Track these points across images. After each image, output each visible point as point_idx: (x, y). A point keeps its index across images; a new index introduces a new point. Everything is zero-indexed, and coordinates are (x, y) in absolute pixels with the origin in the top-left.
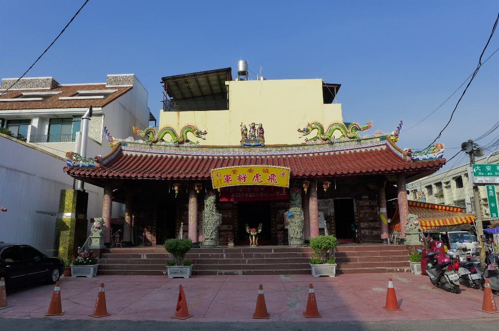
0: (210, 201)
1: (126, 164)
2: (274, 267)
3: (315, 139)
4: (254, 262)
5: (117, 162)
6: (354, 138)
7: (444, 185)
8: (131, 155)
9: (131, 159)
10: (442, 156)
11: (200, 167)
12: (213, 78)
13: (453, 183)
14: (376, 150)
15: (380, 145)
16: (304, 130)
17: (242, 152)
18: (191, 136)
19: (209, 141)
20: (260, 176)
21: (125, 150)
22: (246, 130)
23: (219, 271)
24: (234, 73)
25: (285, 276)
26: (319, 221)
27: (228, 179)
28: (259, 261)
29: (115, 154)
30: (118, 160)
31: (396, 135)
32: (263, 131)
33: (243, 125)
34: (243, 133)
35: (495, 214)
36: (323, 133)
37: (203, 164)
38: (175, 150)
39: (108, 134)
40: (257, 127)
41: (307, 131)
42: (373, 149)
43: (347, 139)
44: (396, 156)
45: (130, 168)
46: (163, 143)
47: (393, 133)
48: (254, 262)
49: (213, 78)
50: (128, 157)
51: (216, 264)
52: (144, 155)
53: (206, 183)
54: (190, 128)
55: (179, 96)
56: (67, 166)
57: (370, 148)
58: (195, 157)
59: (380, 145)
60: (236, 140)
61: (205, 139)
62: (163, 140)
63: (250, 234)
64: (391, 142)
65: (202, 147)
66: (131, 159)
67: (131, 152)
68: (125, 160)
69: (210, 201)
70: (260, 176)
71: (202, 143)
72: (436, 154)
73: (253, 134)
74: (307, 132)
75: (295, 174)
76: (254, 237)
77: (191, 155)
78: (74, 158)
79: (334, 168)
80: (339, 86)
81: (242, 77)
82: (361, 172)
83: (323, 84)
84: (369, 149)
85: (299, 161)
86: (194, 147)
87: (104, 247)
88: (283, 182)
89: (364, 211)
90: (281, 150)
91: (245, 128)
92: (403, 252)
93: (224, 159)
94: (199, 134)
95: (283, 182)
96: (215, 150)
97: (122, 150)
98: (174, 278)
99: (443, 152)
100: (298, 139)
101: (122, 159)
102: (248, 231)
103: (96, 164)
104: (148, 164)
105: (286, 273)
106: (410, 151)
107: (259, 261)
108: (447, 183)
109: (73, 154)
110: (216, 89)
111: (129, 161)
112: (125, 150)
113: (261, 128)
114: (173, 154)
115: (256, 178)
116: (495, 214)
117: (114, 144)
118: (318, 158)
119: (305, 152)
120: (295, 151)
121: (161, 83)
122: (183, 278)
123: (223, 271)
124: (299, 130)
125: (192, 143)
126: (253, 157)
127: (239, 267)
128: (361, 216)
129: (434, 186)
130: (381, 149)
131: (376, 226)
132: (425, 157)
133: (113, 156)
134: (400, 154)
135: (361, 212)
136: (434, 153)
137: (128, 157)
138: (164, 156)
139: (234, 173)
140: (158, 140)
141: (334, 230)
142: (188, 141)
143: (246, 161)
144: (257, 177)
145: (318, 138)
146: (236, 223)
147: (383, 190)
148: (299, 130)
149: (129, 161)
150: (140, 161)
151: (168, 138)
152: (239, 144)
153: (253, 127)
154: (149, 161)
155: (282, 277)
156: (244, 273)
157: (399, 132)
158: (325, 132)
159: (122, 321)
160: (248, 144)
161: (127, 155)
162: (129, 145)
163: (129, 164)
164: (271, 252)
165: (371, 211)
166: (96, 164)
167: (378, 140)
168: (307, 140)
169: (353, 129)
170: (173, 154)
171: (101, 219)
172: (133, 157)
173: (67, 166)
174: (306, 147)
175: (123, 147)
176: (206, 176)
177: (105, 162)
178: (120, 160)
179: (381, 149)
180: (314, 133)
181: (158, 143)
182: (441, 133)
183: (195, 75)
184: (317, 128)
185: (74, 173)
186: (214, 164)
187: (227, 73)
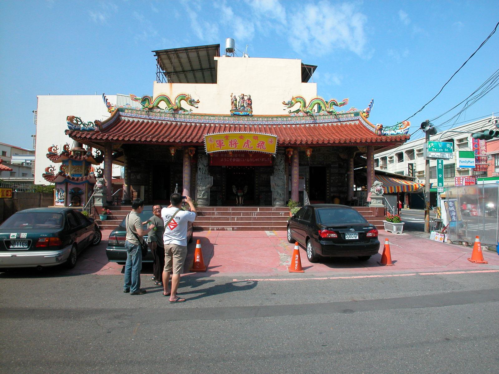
0: (202, 165)
1: (124, 128)
2: (260, 224)
3: (298, 111)
4: (242, 219)
5: (115, 126)
6: (332, 112)
7: (388, 159)
8: (134, 121)
9: (129, 124)
10: (407, 132)
11: (193, 133)
12: (203, 53)
13: (396, 158)
14: (350, 125)
15: (354, 120)
16: (288, 103)
17: (232, 121)
18: (184, 105)
19: (201, 109)
20: (250, 142)
21: (123, 116)
22: (236, 100)
23: (211, 227)
24: (222, 50)
25: (270, 232)
26: (300, 183)
27: (220, 144)
28: (247, 219)
29: (114, 119)
30: (117, 125)
31: (368, 112)
32: (251, 102)
33: (233, 96)
34: (233, 103)
35: (441, 183)
36: (305, 106)
37: (196, 131)
38: (170, 117)
39: (106, 100)
40: (246, 98)
41: (290, 104)
42: (348, 123)
43: (326, 113)
44: (368, 130)
45: (128, 132)
46: (159, 110)
47: (365, 110)
48: (242, 219)
49: (203, 53)
50: (125, 122)
51: (209, 221)
52: (141, 120)
53: (199, 147)
54: (183, 97)
55: (172, 70)
56: (68, 129)
57: (345, 123)
58: (189, 124)
59: (354, 120)
60: (227, 109)
61: (197, 108)
62: (158, 108)
63: (237, 195)
64: (364, 118)
65: (195, 115)
66: (129, 124)
67: (129, 118)
68: (122, 125)
69: (202, 165)
70: (250, 142)
71: (195, 111)
72: (402, 130)
73: (242, 104)
74: (291, 104)
75: (281, 142)
76: (240, 198)
77: (184, 122)
78: (75, 122)
79: (316, 139)
80: (315, 67)
81: (228, 54)
82: (345, 142)
83: (302, 64)
84: (344, 123)
85: (284, 130)
86: (187, 115)
87: (107, 205)
88: (272, 149)
89: (334, 178)
90: (267, 121)
91: (235, 98)
92: (251, 216)
93: (215, 127)
94: (192, 102)
95: (272, 149)
96: (207, 118)
97: (120, 116)
98: (388, 231)
99: (408, 129)
100: (283, 111)
101: (120, 124)
102: (234, 191)
103: (96, 128)
104: (144, 129)
105: (271, 229)
106: (382, 126)
107: (247, 219)
108: (391, 158)
109: (73, 117)
110: (205, 65)
111: (127, 126)
112: (123, 116)
113: (249, 99)
114: (168, 121)
115: (246, 145)
116: (441, 183)
117: (112, 110)
118: (295, 129)
119: (288, 123)
120: (279, 121)
121: (154, 56)
122: (391, 232)
123: (215, 227)
124: (284, 103)
125: (185, 110)
126: (242, 126)
127: (229, 224)
128: (332, 181)
129: (380, 160)
130: (355, 123)
131: (343, 190)
132: (393, 132)
133: (112, 121)
134: (372, 129)
135: (332, 178)
136: (401, 129)
137: (125, 122)
138: (160, 122)
139: (227, 139)
140: (153, 107)
141: (328, 190)
142: (181, 109)
143: (235, 127)
144: (248, 143)
145: (301, 111)
146: (224, 182)
147: (352, 160)
148: (284, 103)
149: (127, 126)
150: (132, 126)
151: (163, 105)
152: (229, 113)
153: (243, 98)
154: (145, 126)
155: (268, 233)
156: (233, 229)
157: (370, 110)
158: (307, 105)
159: (206, 277)
160: (237, 113)
161: (125, 121)
162: (126, 111)
163: (127, 128)
164: (257, 211)
165: (340, 177)
166: (96, 128)
167: (353, 115)
168: (290, 112)
169: (331, 105)
170: (168, 121)
171: (102, 179)
172: (130, 123)
173: (68, 129)
174: (289, 119)
175: (121, 113)
176: (200, 141)
177: (104, 127)
178: (119, 124)
179: (355, 123)
180: (297, 106)
181: (155, 110)
182: (424, 106)
183: (186, 50)
184: (300, 102)
185: (75, 136)
186: (206, 131)
187: (215, 49)
